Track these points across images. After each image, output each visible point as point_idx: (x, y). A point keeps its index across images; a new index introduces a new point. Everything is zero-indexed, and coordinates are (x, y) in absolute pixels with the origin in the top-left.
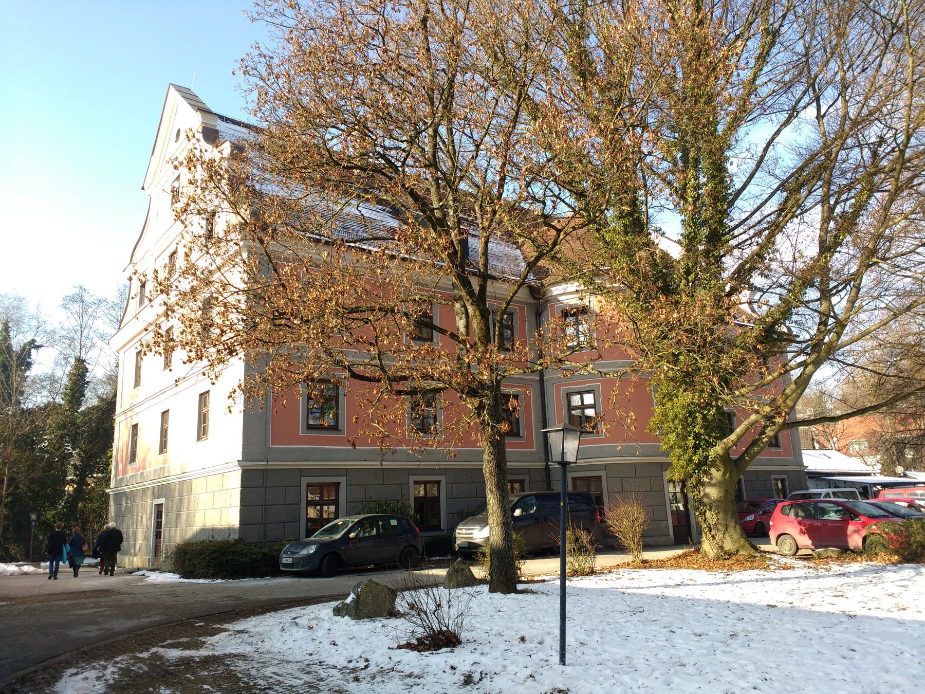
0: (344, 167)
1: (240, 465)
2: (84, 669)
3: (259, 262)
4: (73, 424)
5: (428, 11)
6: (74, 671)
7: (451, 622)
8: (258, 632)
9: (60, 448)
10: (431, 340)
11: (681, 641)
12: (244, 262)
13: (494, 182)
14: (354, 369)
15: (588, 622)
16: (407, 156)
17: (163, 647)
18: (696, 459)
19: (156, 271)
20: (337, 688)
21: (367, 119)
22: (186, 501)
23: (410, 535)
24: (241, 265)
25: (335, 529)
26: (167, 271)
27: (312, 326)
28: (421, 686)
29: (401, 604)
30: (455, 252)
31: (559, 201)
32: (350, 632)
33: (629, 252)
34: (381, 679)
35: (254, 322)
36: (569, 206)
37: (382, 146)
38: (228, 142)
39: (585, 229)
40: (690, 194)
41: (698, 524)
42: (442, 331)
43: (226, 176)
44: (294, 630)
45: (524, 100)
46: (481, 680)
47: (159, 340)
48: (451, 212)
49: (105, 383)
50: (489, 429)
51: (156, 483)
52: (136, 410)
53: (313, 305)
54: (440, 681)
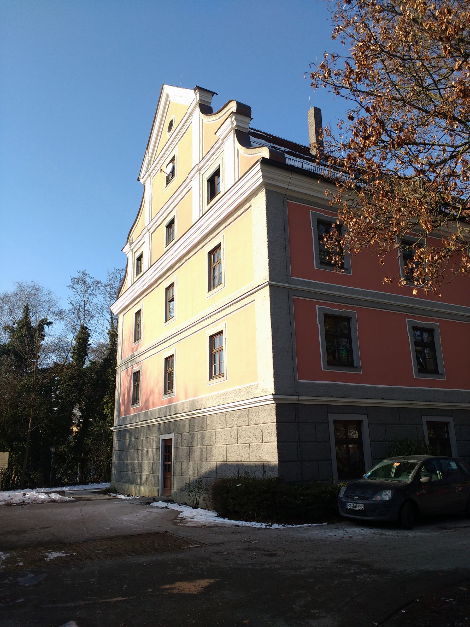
51: (162, 420)
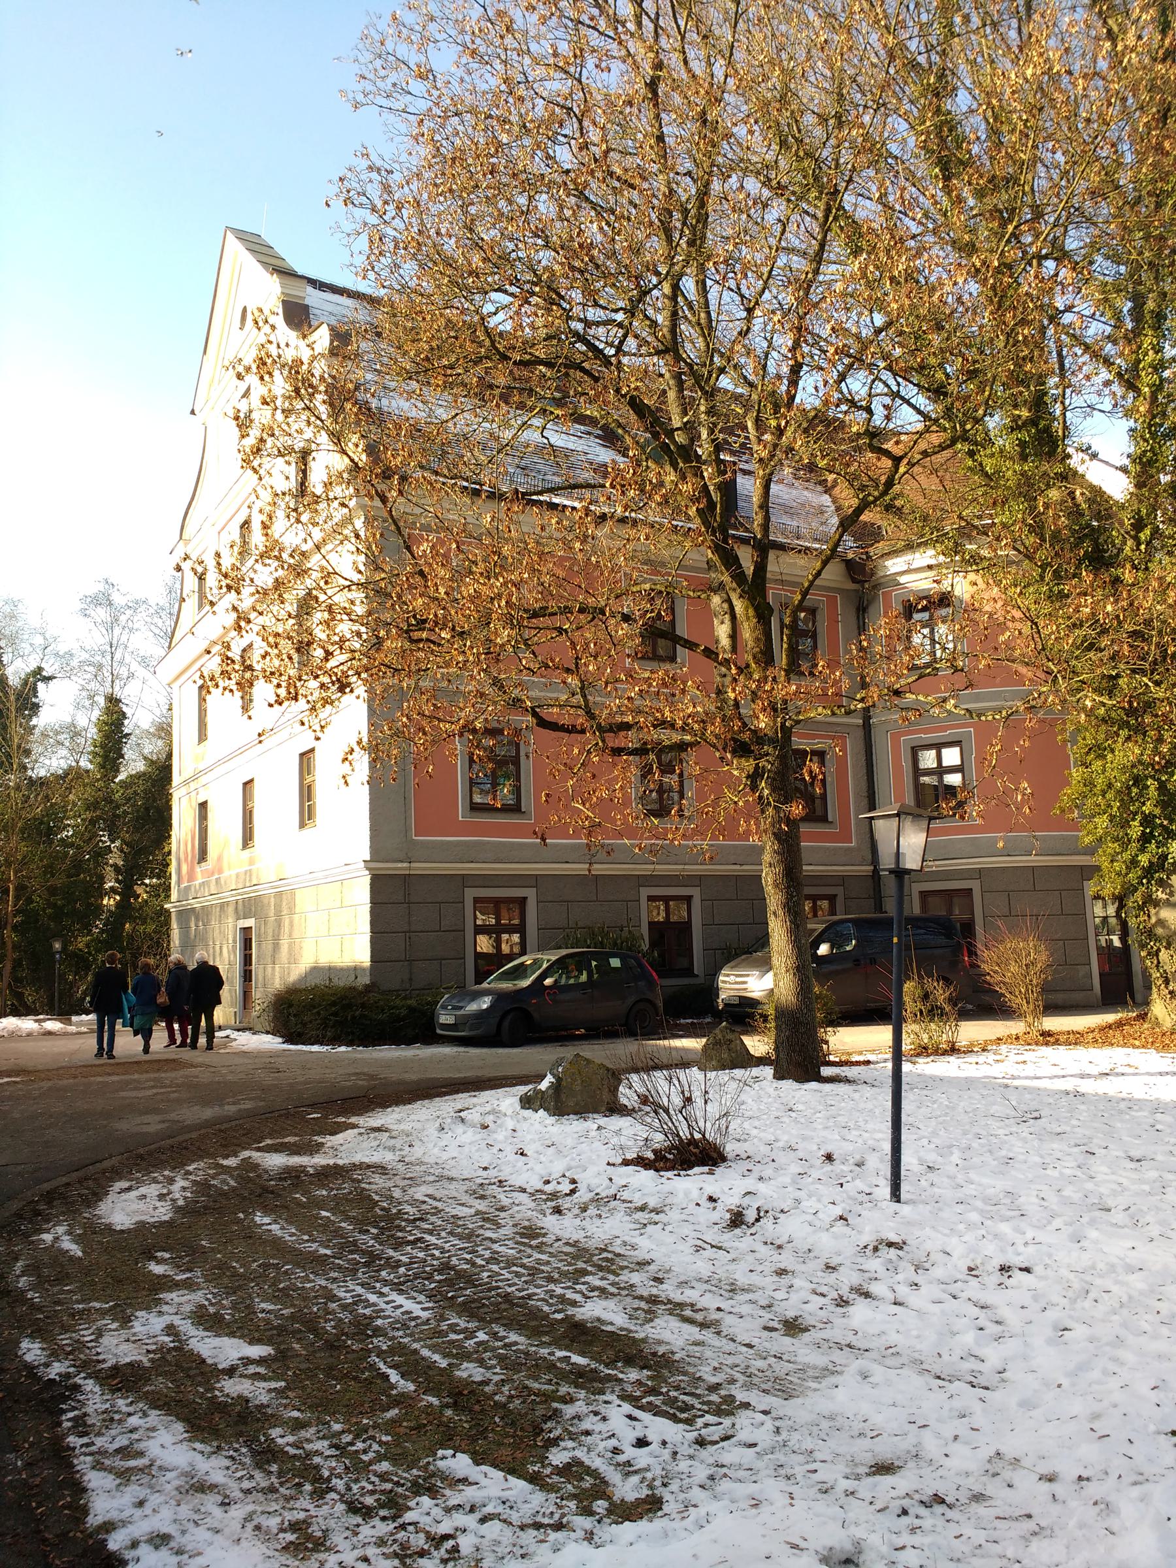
0: (515, 363)
1: (368, 869)
2: (140, 1183)
3: (382, 535)
4: (109, 800)
5: (658, 66)
6: (124, 1184)
7: (709, 1125)
8: (403, 1131)
9: (90, 839)
10: (672, 659)
11: (1104, 1169)
12: (357, 536)
13: (779, 377)
14: (544, 713)
15: (942, 1133)
16: (625, 336)
17: (259, 1149)
18: (1144, 859)
19: (218, 555)
20: (527, 1223)
21: (553, 273)
22: (287, 923)
23: (641, 984)
24: (353, 540)
25: (520, 972)
26: (235, 554)
27: (468, 643)
28: (660, 1226)
29: (627, 1096)
30: (711, 505)
31: (899, 402)
32: (547, 1136)
33: (1028, 489)
34: (596, 1212)
35: (378, 637)
36: (919, 412)
37: (580, 320)
38: (325, 326)
39: (947, 454)
40: (1147, 380)
41: (1145, 970)
42: (690, 645)
43: (322, 388)
44: (460, 1129)
45: (836, 219)
46: (757, 1220)
47: (229, 668)
48: (704, 434)
49: (154, 735)
50: (770, 811)
51: (239, 894)
52: (202, 780)
53: (469, 608)
54: (690, 1218)
